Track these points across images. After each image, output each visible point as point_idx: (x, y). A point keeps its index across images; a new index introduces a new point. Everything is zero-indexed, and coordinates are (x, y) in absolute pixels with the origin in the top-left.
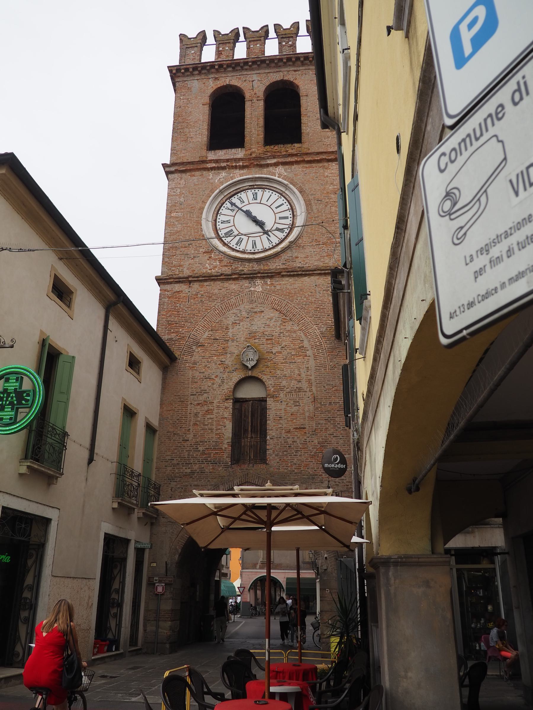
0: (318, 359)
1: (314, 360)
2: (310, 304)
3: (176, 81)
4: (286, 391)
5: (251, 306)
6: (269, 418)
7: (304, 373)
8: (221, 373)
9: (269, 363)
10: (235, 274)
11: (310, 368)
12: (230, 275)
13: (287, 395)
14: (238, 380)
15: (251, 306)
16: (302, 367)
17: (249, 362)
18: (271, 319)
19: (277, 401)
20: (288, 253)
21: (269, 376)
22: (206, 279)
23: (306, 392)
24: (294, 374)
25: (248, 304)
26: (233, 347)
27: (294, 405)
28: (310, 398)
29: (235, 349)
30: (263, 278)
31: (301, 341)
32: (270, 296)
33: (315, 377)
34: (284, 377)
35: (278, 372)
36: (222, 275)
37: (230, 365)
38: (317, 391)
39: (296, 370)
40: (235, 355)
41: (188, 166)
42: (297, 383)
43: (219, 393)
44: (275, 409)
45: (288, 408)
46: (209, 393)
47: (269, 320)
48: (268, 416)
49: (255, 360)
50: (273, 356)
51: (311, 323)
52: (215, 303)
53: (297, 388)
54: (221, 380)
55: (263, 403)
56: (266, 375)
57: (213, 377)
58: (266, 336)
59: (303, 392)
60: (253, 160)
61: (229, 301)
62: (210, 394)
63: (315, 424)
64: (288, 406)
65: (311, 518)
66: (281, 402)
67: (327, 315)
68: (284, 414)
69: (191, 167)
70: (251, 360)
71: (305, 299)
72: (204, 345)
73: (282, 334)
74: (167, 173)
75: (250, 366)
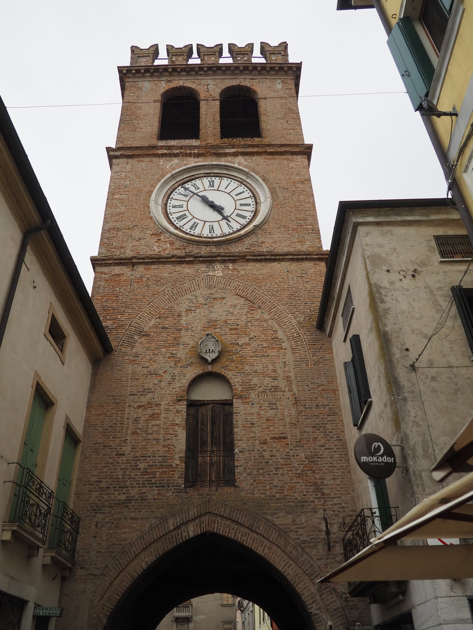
0: (297, 353)
1: (293, 353)
2: (282, 291)
5: (209, 291)
7: (280, 369)
8: (171, 367)
9: (235, 356)
10: (189, 256)
11: (287, 363)
12: (184, 257)
13: (260, 396)
14: (194, 376)
15: (209, 291)
16: (278, 362)
17: (208, 354)
18: (235, 306)
19: (247, 403)
21: (234, 372)
22: (154, 262)
23: (284, 391)
24: (268, 370)
25: (206, 289)
26: (187, 337)
27: (269, 408)
28: (291, 399)
29: (190, 339)
30: (224, 263)
32: (233, 281)
33: (295, 374)
34: (254, 373)
35: (247, 367)
37: (183, 358)
38: (299, 391)
39: (270, 364)
40: (190, 346)
41: (136, 151)
43: (168, 392)
44: (244, 413)
45: (262, 412)
49: (216, 352)
51: (286, 311)
52: (164, 287)
53: (272, 386)
54: (172, 376)
56: (231, 370)
57: (161, 372)
59: (280, 391)
60: (209, 148)
61: (182, 286)
63: (299, 432)
64: (262, 410)
66: (253, 404)
68: (257, 420)
69: (140, 152)
70: (211, 351)
71: (276, 286)
72: (149, 335)
73: (249, 323)
74: (111, 158)
75: (210, 359)
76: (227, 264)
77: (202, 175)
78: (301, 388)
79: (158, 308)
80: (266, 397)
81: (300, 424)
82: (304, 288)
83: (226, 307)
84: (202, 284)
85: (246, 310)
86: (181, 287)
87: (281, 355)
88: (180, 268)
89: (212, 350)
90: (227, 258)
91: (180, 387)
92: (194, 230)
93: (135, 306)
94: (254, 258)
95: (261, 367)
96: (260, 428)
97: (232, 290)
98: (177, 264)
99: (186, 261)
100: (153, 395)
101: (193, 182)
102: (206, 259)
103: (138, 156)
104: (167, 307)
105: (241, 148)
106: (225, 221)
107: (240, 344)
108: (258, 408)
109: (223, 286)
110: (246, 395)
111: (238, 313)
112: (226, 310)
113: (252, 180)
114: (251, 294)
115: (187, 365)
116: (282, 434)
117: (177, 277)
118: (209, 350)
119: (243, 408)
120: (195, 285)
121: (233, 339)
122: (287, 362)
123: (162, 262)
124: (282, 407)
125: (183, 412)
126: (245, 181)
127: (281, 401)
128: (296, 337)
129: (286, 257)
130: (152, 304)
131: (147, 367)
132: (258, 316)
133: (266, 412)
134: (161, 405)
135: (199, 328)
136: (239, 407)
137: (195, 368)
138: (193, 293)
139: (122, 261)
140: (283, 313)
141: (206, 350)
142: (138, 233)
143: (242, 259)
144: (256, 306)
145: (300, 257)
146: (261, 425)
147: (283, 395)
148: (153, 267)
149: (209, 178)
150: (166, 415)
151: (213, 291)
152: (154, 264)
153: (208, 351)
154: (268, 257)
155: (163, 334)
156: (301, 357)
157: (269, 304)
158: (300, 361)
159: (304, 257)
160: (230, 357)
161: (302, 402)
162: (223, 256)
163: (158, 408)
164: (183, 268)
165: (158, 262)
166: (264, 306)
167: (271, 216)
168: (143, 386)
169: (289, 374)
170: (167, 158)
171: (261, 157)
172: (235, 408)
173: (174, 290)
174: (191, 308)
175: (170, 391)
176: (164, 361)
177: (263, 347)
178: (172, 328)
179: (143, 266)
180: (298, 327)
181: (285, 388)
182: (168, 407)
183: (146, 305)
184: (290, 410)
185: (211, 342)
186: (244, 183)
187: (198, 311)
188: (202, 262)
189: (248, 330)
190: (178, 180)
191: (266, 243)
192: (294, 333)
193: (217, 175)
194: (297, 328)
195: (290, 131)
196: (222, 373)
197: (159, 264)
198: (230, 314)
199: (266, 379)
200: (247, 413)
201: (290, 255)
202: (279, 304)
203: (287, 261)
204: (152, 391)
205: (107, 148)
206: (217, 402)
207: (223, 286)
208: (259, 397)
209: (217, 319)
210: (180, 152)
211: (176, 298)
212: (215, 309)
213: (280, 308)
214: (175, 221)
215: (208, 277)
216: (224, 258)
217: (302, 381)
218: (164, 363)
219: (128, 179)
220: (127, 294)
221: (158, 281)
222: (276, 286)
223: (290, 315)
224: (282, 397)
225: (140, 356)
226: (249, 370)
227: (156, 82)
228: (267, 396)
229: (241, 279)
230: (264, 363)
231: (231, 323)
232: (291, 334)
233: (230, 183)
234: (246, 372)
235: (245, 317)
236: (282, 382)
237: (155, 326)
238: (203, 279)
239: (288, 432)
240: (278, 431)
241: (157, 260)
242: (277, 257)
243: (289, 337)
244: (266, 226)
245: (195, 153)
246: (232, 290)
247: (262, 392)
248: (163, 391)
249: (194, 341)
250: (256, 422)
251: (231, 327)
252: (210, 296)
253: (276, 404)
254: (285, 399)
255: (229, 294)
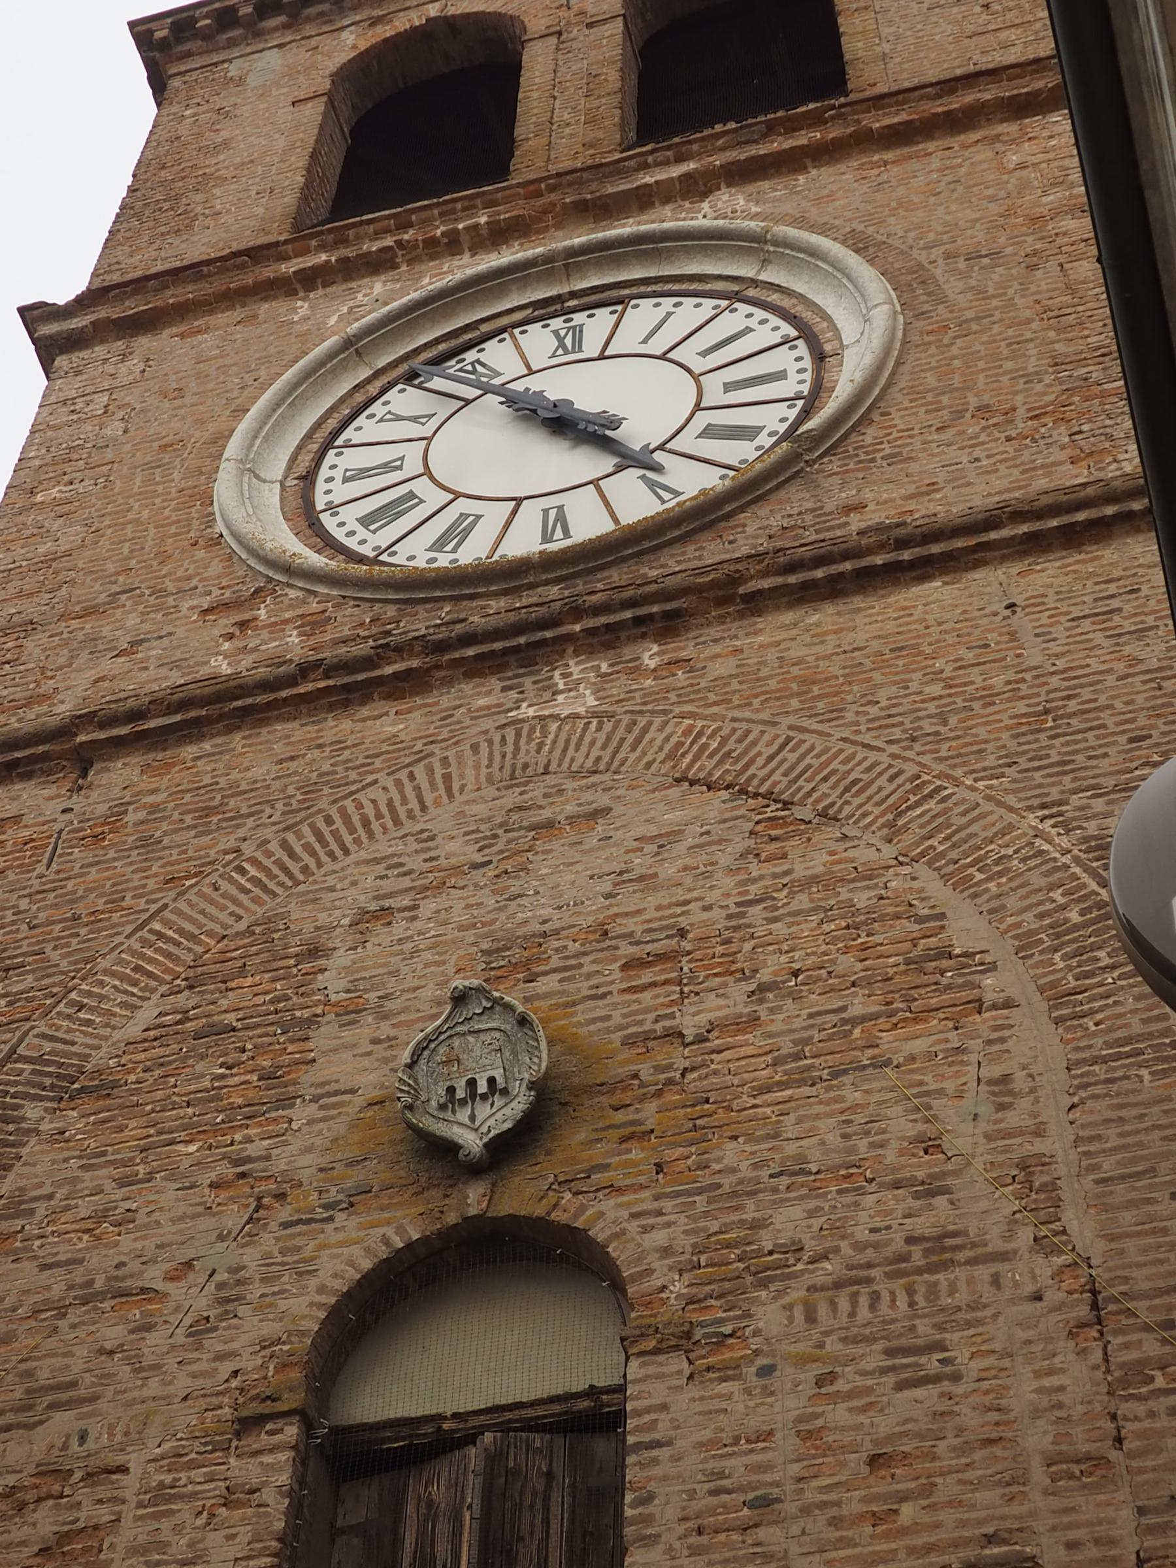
0: (1092, 1012)
1: (1058, 1021)
2: (976, 705)
3: (170, 72)
4: (808, 1280)
5: (512, 798)
6: (648, 1520)
7: (968, 1127)
8: (221, 1238)
9: (651, 1107)
10: (400, 650)
11: (1020, 1082)
12: (368, 663)
13: (823, 1311)
14: (367, 1264)
15: (512, 798)
16: (950, 1086)
17: (463, 1115)
18: (665, 840)
19: (729, 1372)
20: (789, 500)
21: (646, 1194)
22: (196, 722)
23: (1003, 1256)
24: (882, 1145)
25: (490, 792)
26: (347, 1055)
27: (890, 1380)
28: (1053, 1296)
29: (365, 1062)
30: (609, 646)
31: (921, 920)
32: (658, 721)
33: (1078, 1141)
34: (785, 1181)
35: (731, 1153)
36: (305, 670)
37: (305, 1176)
38: (1113, 1238)
39: (896, 1111)
40: (359, 1101)
41: (169, 292)
42: (912, 1203)
43: (183, 1384)
44: (707, 1434)
45: (839, 1414)
46: (94, 1399)
47: (653, 848)
48: (636, 1504)
49: (516, 1088)
50: (680, 1058)
51: (1000, 804)
52: (241, 833)
53: (910, 1240)
54: (221, 1286)
55: (601, 1446)
56: (620, 1191)
57: (153, 1277)
58: (623, 944)
59: (972, 1262)
60: (552, 189)
61: (348, 803)
62: (102, 1405)
63: (1127, 1514)
64: (835, 1398)
65: (607, 353)
66: (766, 1371)
67: (1123, 739)
68: (795, 1469)
69: (188, 292)
70: (482, 1087)
71: (935, 689)
72: (115, 1085)
73: (756, 911)
75: (472, 1141)
76: (628, 652)
77: (518, 316)
78: (1127, 1217)
79: (191, 937)
80: (864, 1313)
81: (1131, 1455)
82: (1120, 667)
83: (608, 851)
84: (470, 773)
85: (741, 844)
86: (343, 812)
87: (975, 1044)
88: (346, 725)
89: (492, 1081)
90: (628, 614)
91: (265, 1344)
92: (454, 550)
93: (55, 956)
94: (792, 579)
95: (834, 1139)
96: (818, 1525)
97: (649, 765)
98: (331, 707)
99: (380, 681)
100: (80, 1418)
101: (471, 356)
102: (498, 646)
103: (182, 311)
104: (242, 926)
105: (723, 149)
106: (633, 473)
107: (690, 1033)
108: (808, 1389)
109: (595, 753)
110: (721, 1322)
111: (686, 868)
112: (607, 868)
113: (793, 265)
114: (771, 758)
115: (326, 1207)
116: (990, 1539)
117: (326, 767)
118: (472, 1083)
119: (697, 1407)
120: (425, 786)
121: (647, 1011)
122: (1020, 1075)
123: (246, 712)
124: (990, 1361)
125: (268, 1495)
126: (755, 283)
127: (980, 1322)
128: (1077, 927)
129: (993, 535)
130: (157, 926)
131: (69, 1262)
132: (818, 862)
133: (864, 1410)
134: (123, 1470)
135: (429, 992)
136: (664, 1407)
137: (376, 1216)
138: (409, 827)
139: (18, 755)
140: (982, 816)
141: (451, 1090)
142: (132, 620)
143: (721, 602)
144: (799, 812)
145: (1081, 516)
146: (824, 1505)
147: (996, 1281)
148: (190, 751)
149: (557, 323)
150: (152, 1525)
151: (536, 792)
152: (201, 737)
153: (460, 1094)
154: (879, 560)
155: (200, 1067)
156: (1121, 1034)
157: (890, 788)
158: (1118, 1057)
159: (1110, 510)
160: (620, 1117)
161: (1140, 1306)
162: (597, 610)
163: (103, 1492)
164: (364, 720)
165: (221, 717)
166: (857, 801)
167: (903, 381)
168: (29, 1374)
169: (1039, 1146)
170: (331, 290)
171: (842, 167)
172: (638, 1413)
173: (300, 836)
174: (386, 903)
175: (194, 1376)
176: (182, 1208)
177: (845, 1021)
178: (257, 1026)
179: (136, 760)
180: (1077, 860)
181: (1009, 1236)
182: (168, 1479)
183: (117, 940)
184: (1051, 1372)
185: (487, 1037)
186: (751, 293)
187: (428, 907)
188: (477, 669)
189: (748, 946)
190: (382, 362)
191: (871, 507)
192: (1063, 908)
193: (594, 299)
194: (1085, 878)
195: (1003, 35)
196: (557, 1216)
197: (230, 730)
198: (631, 887)
199: (870, 1200)
200: (726, 1438)
201: (1018, 516)
202: (958, 773)
203: (1004, 559)
204: (82, 1392)
205: (23, 311)
206: (529, 1413)
207: (595, 753)
208: (811, 1318)
209: (546, 927)
210: (399, 243)
211: (305, 870)
212: (542, 878)
213: (961, 793)
214: (351, 534)
215: (510, 733)
216: (603, 620)
217: (1139, 1175)
218: (181, 1219)
219: (121, 414)
220: (24, 904)
221: (209, 811)
222: (935, 689)
223: (1032, 819)
224: (988, 1294)
225: (41, 1209)
226: (744, 1165)
227: (314, 42)
228: (872, 1307)
229: (712, 697)
230: (854, 1108)
231: (639, 929)
232: (1041, 916)
233: (669, 314)
234: (727, 1182)
235: (729, 882)
236: (983, 1205)
237: (157, 1034)
238: (475, 748)
239: (1040, 1526)
240: (962, 1524)
241: (215, 709)
242: (936, 549)
243: (1030, 933)
244: (870, 434)
245: (476, 226)
246: (649, 765)
247: (838, 1285)
248: (154, 1383)
249: (386, 1070)
250: (789, 1487)
251: (634, 949)
252: (515, 817)
253: (941, 1347)
254: (1013, 1301)
255: (631, 788)
